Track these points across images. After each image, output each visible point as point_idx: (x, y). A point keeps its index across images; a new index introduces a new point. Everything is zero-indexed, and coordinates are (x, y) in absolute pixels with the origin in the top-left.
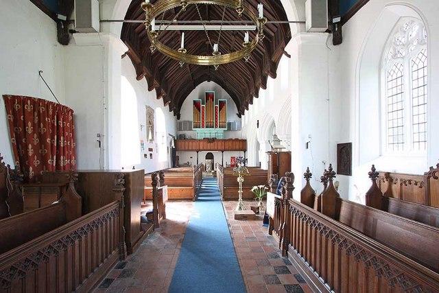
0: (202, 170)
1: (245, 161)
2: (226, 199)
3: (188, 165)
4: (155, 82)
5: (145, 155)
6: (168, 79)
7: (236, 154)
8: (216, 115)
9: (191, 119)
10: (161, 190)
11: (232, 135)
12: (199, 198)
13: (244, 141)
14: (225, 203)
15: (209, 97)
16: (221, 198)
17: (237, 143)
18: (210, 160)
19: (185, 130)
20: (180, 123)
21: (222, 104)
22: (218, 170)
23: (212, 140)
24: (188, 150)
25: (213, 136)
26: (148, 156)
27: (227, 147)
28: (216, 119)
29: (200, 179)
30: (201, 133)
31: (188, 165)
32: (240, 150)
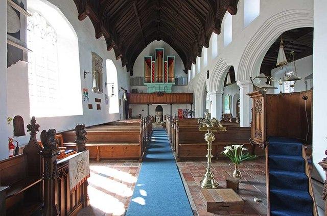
0: (152, 122)
1: (192, 113)
2: (181, 159)
3: (139, 117)
4: (103, 29)
5: (90, 107)
6: (119, 33)
7: (183, 107)
8: (165, 71)
9: (143, 76)
10: (260, 73)
11: (179, 90)
12: (149, 156)
13: (191, 95)
14: (182, 166)
15: (159, 53)
16: (174, 155)
17: (185, 96)
18: (159, 113)
19: (137, 85)
20: (133, 79)
21: (171, 60)
22: (168, 122)
23: (161, 94)
24: (140, 103)
25: (162, 90)
26: (95, 107)
27: (175, 100)
28: (165, 74)
29: (150, 131)
30: (151, 87)
31: (139, 117)
32: (186, 103)
